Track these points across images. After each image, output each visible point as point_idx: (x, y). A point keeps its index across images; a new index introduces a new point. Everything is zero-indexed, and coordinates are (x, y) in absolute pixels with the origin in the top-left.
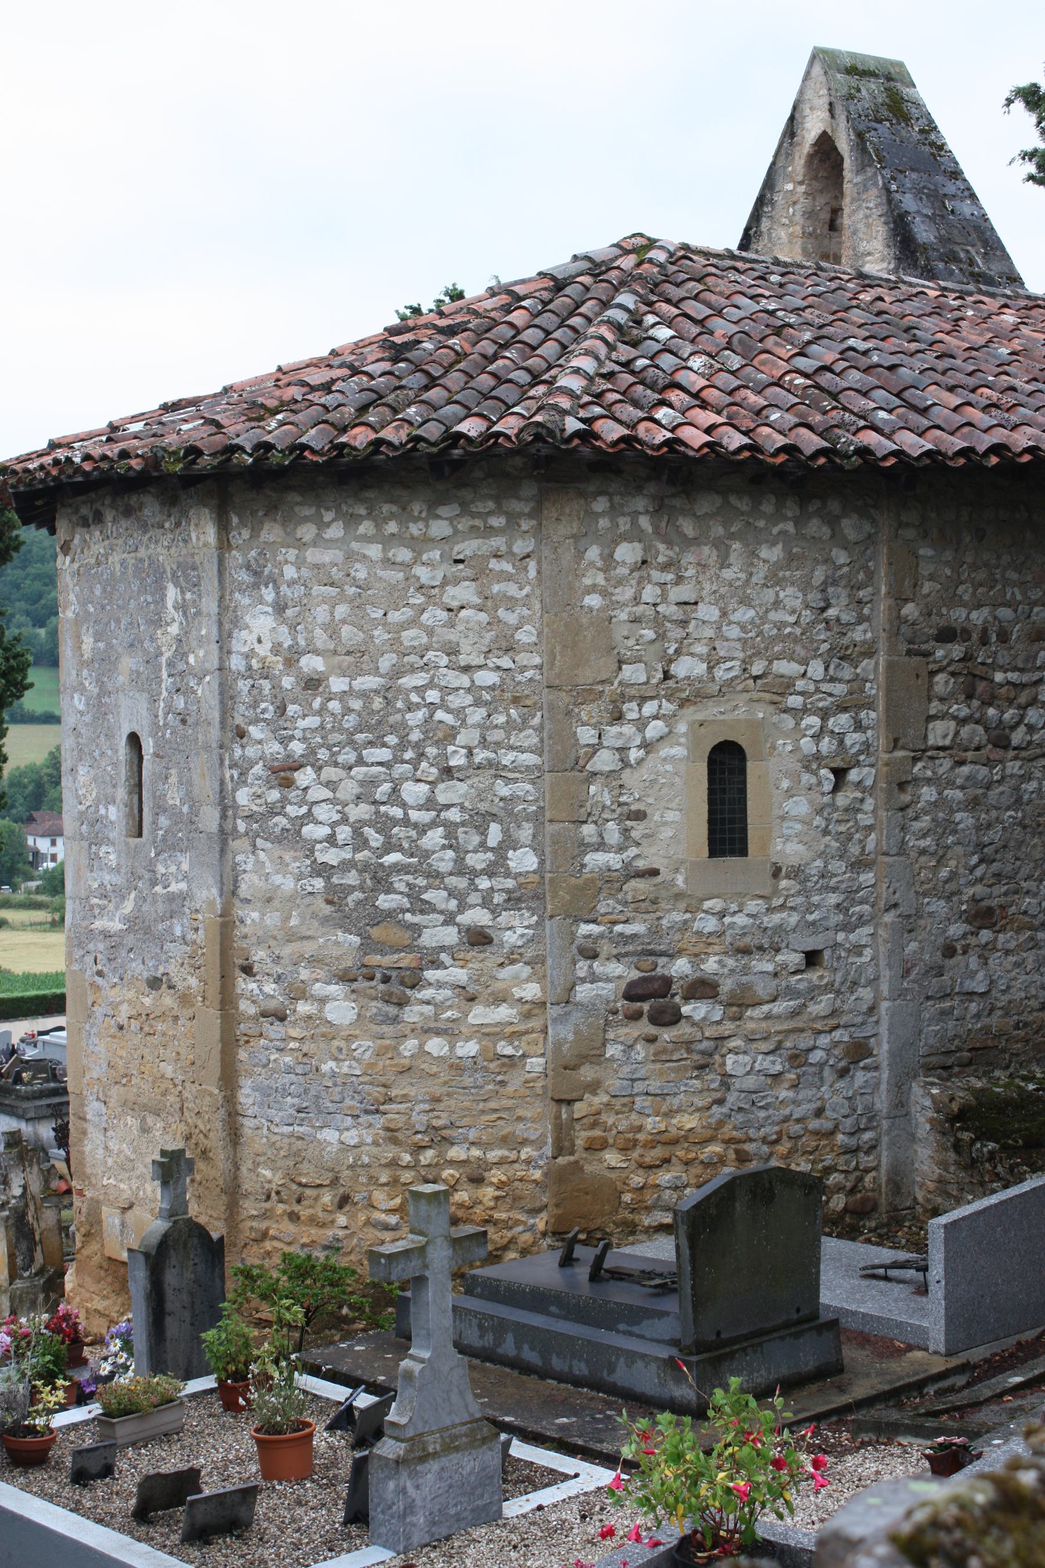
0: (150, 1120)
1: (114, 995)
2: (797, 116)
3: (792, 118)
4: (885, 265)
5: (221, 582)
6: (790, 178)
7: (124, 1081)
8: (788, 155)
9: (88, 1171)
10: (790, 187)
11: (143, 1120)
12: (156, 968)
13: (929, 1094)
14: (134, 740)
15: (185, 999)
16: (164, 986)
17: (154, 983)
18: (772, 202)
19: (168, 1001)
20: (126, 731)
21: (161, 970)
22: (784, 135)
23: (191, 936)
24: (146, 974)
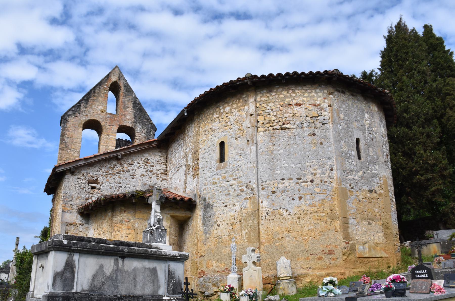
0: (371, 222)
1: (358, 193)
2: (110, 75)
3: (108, 75)
4: (133, 111)
5: (117, 105)
6: (106, 86)
7: (362, 213)
8: (106, 81)
9: (351, 236)
10: (106, 87)
11: (369, 222)
12: (371, 188)
13: (227, 271)
14: (358, 141)
15: (380, 195)
16: (374, 192)
17: (371, 191)
18: (100, 88)
19: (375, 195)
20: (356, 137)
21: (373, 188)
22: (106, 77)
23: (379, 182)
24: (368, 189)
